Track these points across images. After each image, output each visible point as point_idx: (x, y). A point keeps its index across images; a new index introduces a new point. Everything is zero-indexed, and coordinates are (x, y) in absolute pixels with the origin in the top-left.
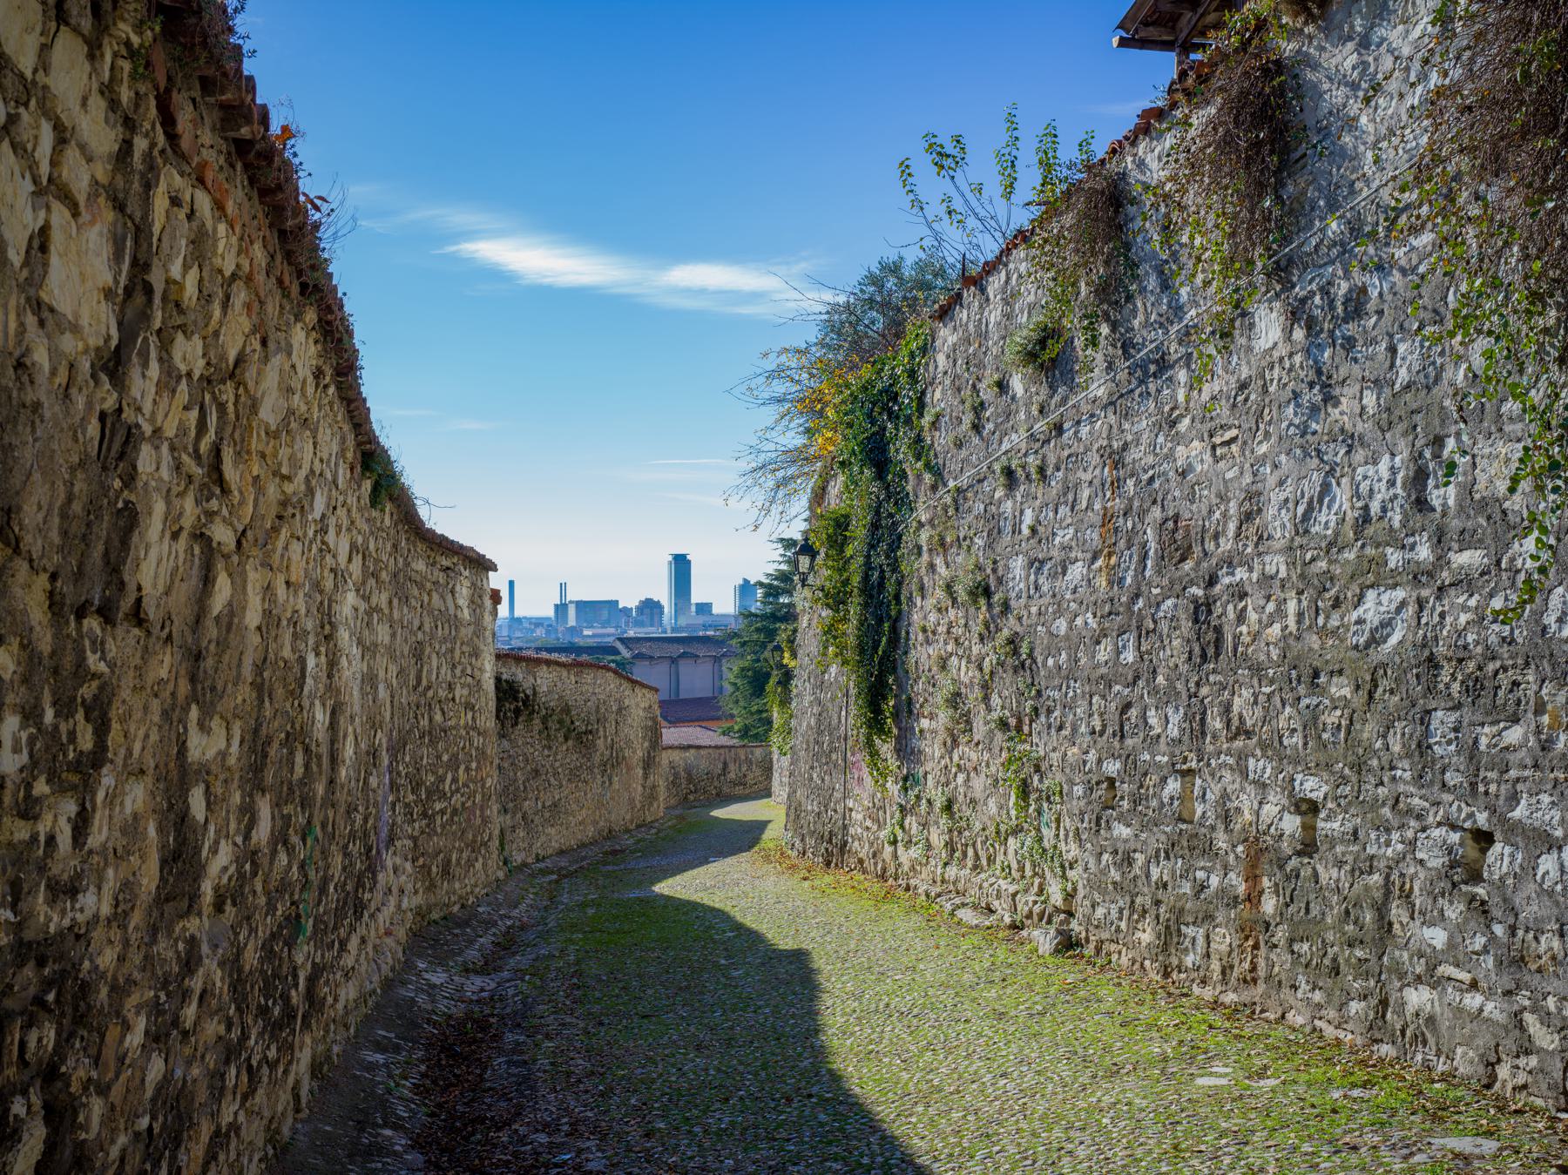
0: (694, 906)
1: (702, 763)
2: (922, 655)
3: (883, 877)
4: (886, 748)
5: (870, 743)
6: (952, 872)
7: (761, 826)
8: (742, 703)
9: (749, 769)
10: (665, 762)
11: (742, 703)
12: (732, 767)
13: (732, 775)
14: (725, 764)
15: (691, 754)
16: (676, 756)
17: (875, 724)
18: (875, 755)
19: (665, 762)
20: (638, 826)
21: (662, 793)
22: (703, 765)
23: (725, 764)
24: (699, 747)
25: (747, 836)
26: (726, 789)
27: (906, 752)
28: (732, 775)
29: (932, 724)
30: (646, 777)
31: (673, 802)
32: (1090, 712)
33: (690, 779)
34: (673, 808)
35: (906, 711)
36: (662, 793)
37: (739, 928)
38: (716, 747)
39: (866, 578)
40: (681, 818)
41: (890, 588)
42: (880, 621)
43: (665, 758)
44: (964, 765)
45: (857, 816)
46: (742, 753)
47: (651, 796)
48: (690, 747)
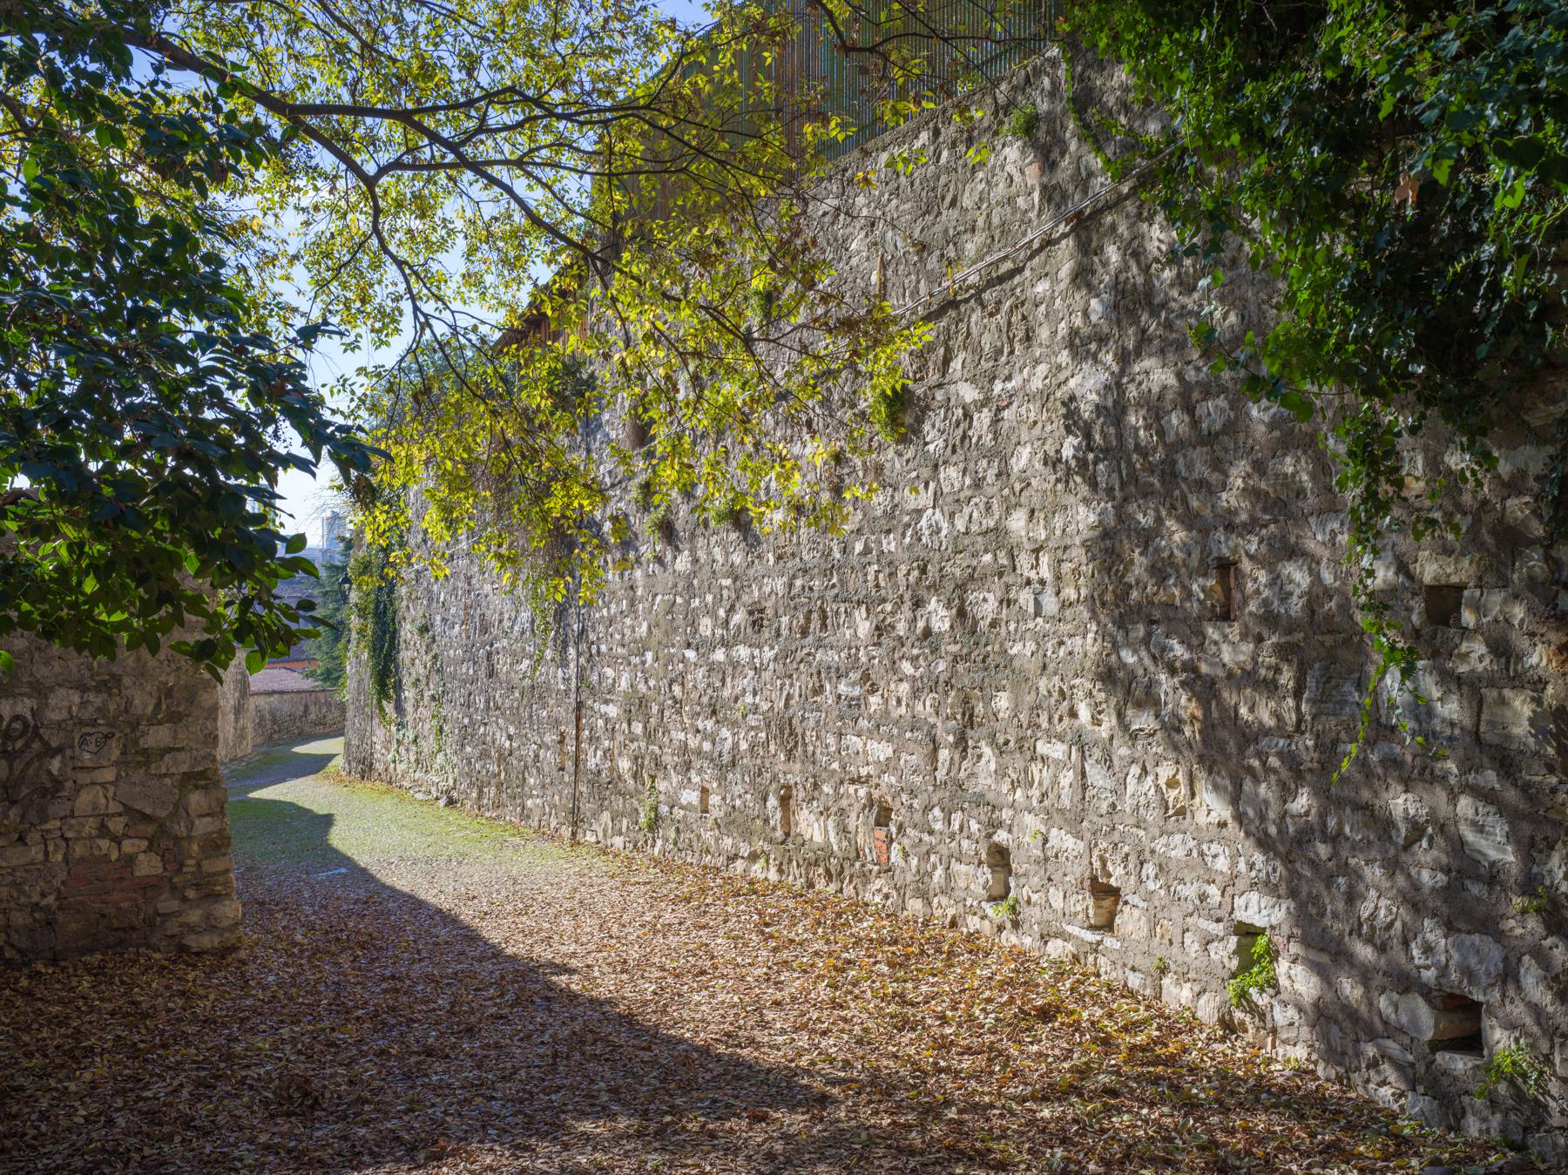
0: (274, 802)
1: (286, 707)
2: (405, 655)
3: (390, 783)
4: (389, 707)
5: (380, 702)
6: (418, 775)
7: (329, 758)
8: (325, 648)
9: (329, 710)
10: (252, 707)
11: (325, 648)
12: (312, 708)
13: (313, 717)
14: (306, 707)
15: (274, 699)
16: (261, 701)
17: (382, 692)
18: (382, 709)
19: (252, 707)
20: (231, 760)
21: (250, 734)
22: (287, 708)
23: (306, 707)
24: (282, 693)
25: (317, 764)
26: (307, 729)
27: (399, 709)
28: (313, 717)
29: (409, 694)
30: (237, 720)
31: (259, 740)
32: (459, 696)
33: (274, 720)
34: (260, 746)
35: (399, 687)
36: (250, 734)
37: (300, 808)
38: (298, 692)
39: (377, 607)
40: (267, 754)
41: (390, 614)
42: (384, 633)
43: (252, 703)
44: (420, 717)
45: (378, 747)
46: (322, 697)
47: (241, 737)
48: (274, 692)
